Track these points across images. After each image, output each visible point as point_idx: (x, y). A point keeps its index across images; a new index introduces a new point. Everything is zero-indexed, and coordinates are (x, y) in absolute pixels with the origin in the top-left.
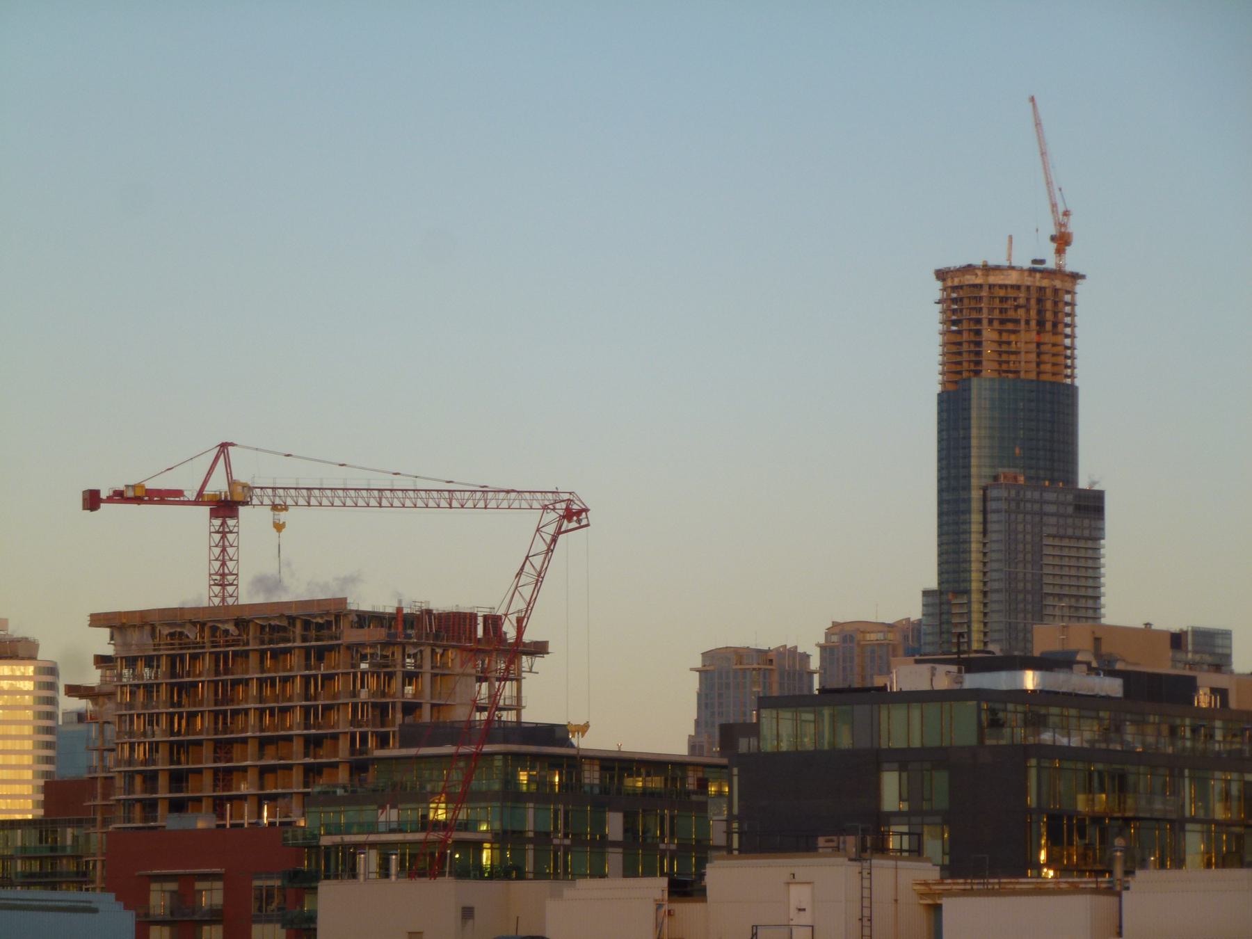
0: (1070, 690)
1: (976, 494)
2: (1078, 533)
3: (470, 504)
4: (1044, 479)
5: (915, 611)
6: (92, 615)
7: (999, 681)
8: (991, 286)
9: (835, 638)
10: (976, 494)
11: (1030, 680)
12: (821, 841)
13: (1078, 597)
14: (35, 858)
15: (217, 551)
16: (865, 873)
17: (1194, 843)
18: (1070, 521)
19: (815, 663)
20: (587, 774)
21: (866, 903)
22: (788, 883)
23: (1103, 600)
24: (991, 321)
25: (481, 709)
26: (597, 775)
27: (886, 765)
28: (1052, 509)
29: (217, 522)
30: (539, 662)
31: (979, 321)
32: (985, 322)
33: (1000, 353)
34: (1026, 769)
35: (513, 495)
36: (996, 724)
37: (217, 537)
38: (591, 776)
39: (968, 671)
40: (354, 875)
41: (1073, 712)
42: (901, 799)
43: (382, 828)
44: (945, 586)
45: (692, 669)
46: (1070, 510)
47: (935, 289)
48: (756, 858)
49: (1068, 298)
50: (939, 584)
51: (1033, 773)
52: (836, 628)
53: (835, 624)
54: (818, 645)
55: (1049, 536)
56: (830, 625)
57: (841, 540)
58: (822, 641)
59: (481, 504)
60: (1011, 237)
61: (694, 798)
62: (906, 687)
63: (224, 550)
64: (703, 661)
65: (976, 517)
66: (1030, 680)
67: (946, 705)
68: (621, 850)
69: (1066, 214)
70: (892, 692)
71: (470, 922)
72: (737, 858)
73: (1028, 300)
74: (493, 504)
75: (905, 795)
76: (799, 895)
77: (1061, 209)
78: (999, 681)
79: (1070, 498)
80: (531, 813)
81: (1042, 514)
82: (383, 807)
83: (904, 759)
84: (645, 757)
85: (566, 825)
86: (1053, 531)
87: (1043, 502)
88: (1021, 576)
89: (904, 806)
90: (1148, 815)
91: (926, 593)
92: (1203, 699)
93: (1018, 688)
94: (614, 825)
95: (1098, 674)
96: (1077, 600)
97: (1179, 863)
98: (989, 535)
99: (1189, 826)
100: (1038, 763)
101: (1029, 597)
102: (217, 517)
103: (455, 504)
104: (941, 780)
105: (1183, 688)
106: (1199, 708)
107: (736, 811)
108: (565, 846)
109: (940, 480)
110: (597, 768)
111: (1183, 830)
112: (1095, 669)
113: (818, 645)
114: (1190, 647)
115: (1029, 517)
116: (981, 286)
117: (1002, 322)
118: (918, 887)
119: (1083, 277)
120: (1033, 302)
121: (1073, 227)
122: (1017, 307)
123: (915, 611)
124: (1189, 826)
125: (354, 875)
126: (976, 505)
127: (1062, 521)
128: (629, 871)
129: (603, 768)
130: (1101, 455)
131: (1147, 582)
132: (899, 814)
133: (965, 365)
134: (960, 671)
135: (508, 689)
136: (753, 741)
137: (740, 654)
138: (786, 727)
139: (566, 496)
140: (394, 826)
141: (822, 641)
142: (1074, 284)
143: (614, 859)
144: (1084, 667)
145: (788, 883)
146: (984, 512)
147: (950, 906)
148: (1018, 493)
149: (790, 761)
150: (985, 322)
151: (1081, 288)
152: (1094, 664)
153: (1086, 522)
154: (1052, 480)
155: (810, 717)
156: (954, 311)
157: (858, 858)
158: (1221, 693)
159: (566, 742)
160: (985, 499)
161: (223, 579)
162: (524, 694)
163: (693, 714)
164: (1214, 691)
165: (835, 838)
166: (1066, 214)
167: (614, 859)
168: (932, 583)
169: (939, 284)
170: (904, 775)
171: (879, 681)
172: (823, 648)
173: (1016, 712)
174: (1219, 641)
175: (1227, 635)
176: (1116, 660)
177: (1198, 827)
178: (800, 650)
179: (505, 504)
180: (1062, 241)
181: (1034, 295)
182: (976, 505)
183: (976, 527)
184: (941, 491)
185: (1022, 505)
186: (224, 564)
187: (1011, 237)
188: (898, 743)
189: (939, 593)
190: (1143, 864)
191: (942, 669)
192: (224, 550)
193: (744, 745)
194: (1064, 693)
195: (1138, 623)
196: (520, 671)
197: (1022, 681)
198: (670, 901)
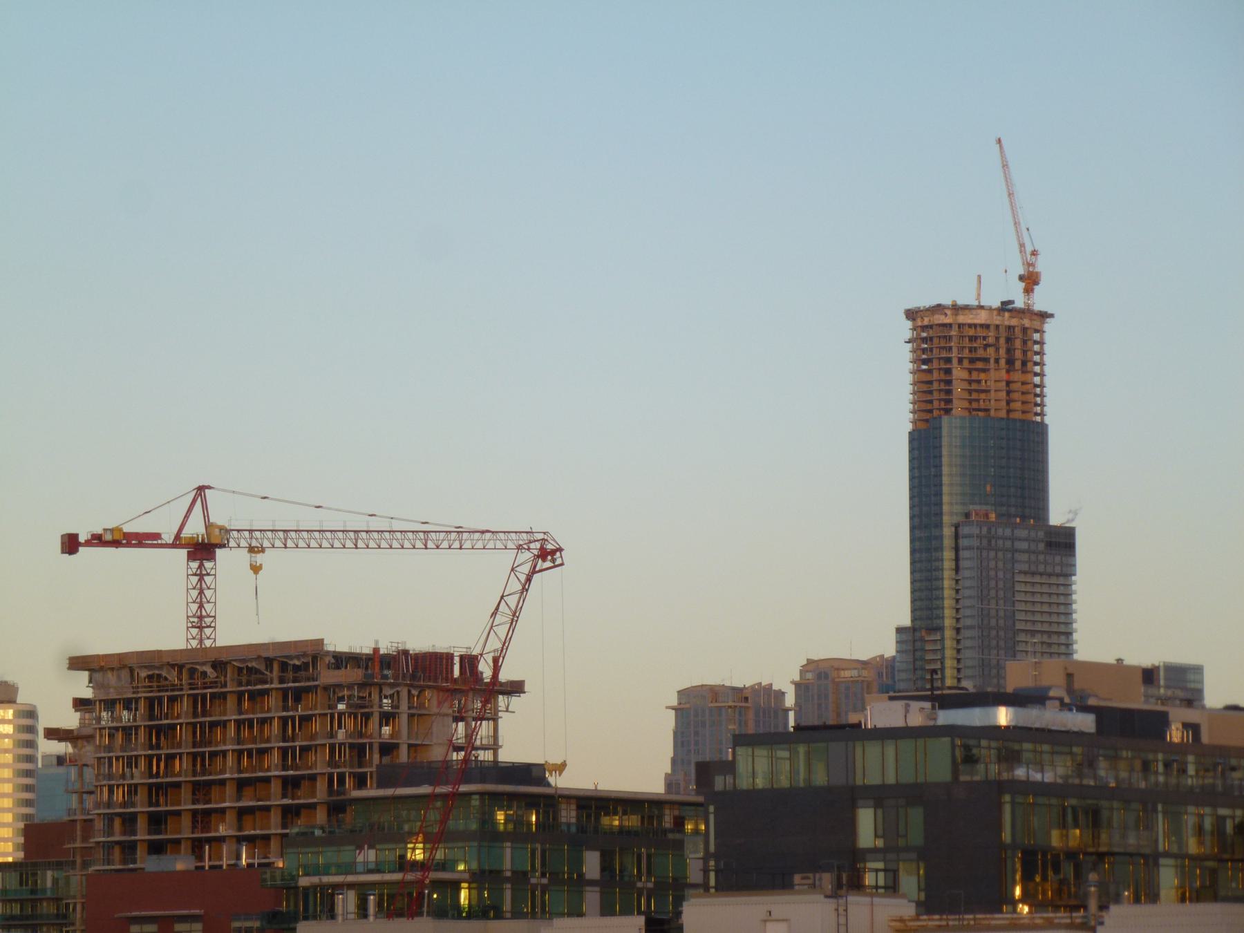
0: (1043, 726)
1: (948, 532)
3: (445, 544)
4: (1016, 516)
5: (888, 647)
6: (63, 552)
7: (972, 717)
8: (960, 325)
9: (809, 676)
10: (948, 532)
11: (1003, 716)
12: (797, 878)
13: (1049, 633)
14: (16, 901)
15: (195, 593)
16: (841, 909)
17: (1168, 878)
18: (1041, 557)
19: (790, 701)
20: (564, 813)
22: (765, 921)
23: (1075, 636)
24: (960, 361)
25: (458, 749)
26: (574, 813)
27: (860, 802)
28: (1024, 545)
29: (195, 565)
30: (515, 701)
31: (948, 360)
32: (955, 361)
33: (970, 392)
34: (1000, 806)
35: (488, 535)
36: (970, 760)
37: (195, 579)
38: (568, 815)
39: (942, 707)
40: (332, 915)
42: (876, 836)
43: (360, 868)
44: (918, 623)
45: (667, 708)
46: (1041, 546)
47: (905, 329)
48: (754, 899)
49: (1036, 336)
51: (1007, 809)
53: (810, 662)
54: (793, 682)
55: (1020, 572)
56: (805, 662)
57: (815, 578)
58: (797, 678)
59: (457, 545)
61: (670, 836)
63: (201, 592)
64: (679, 699)
65: (948, 555)
66: (1003, 716)
67: (920, 742)
68: (597, 889)
73: (997, 339)
74: (467, 545)
75: (880, 832)
77: (1029, 249)
78: (972, 717)
79: (1041, 534)
80: (508, 851)
81: (1014, 551)
82: (361, 848)
83: (879, 796)
85: (543, 864)
86: (1025, 567)
89: (880, 843)
90: (1122, 850)
91: (899, 630)
92: (1175, 734)
93: (991, 723)
95: (1071, 710)
96: (1050, 637)
99: (1162, 861)
101: (1002, 633)
102: (194, 560)
103: (430, 544)
104: (916, 816)
106: (1171, 744)
107: (712, 848)
109: (912, 518)
110: (574, 807)
111: (1157, 865)
112: (1067, 705)
113: (793, 682)
114: (1162, 682)
116: (950, 325)
118: (893, 924)
119: (1052, 316)
120: (1002, 341)
121: (1041, 266)
122: (986, 346)
123: (888, 647)
124: (1162, 861)
125: (332, 915)
126: (948, 542)
127: (1033, 557)
128: (607, 910)
129: (579, 807)
130: (1073, 490)
131: (1116, 619)
132: (875, 850)
133: (936, 403)
135: (485, 729)
136: (729, 779)
137: (714, 692)
138: (762, 765)
139: (541, 536)
140: (372, 866)
141: (797, 678)
143: (592, 897)
144: (1057, 703)
146: (957, 549)
150: (955, 361)
151: (1049, 326)
152: (1067, 700)
153: (1058, 559)
154: (1023, 517)
155: (786, 754)
156: (924, 351)
157: (834, 895)
158: (1193, 728)
159: (543, 781)
160: (957, 536)
161: (200, 622)
163: (669, 752)
164: (1186, 726)
165: (811, 875)
166: (1034, 253)
167: (592, 897)
168: (906, 621)
169: (909, 324)
170: (880, 812)
171: (853, 718)
173: (989, 748)
174: (1191, 677)
175: (1198, 670)
176: (1090, 696)
177: (1171, 861)
178: (775, 687)
179: (480, 545)
180: (1030, 280)
183: (948, 564)
184: (913, 529)
185: (993, 542)
186: (201, 606)
188: (873, 779)
189: (913, 629)
190: (1117, 899)
191: (915, 705)
192: (201, 592)
193: (720, 783)
194: (1037, 729)
196: (496, 711)
197: (995, 716)
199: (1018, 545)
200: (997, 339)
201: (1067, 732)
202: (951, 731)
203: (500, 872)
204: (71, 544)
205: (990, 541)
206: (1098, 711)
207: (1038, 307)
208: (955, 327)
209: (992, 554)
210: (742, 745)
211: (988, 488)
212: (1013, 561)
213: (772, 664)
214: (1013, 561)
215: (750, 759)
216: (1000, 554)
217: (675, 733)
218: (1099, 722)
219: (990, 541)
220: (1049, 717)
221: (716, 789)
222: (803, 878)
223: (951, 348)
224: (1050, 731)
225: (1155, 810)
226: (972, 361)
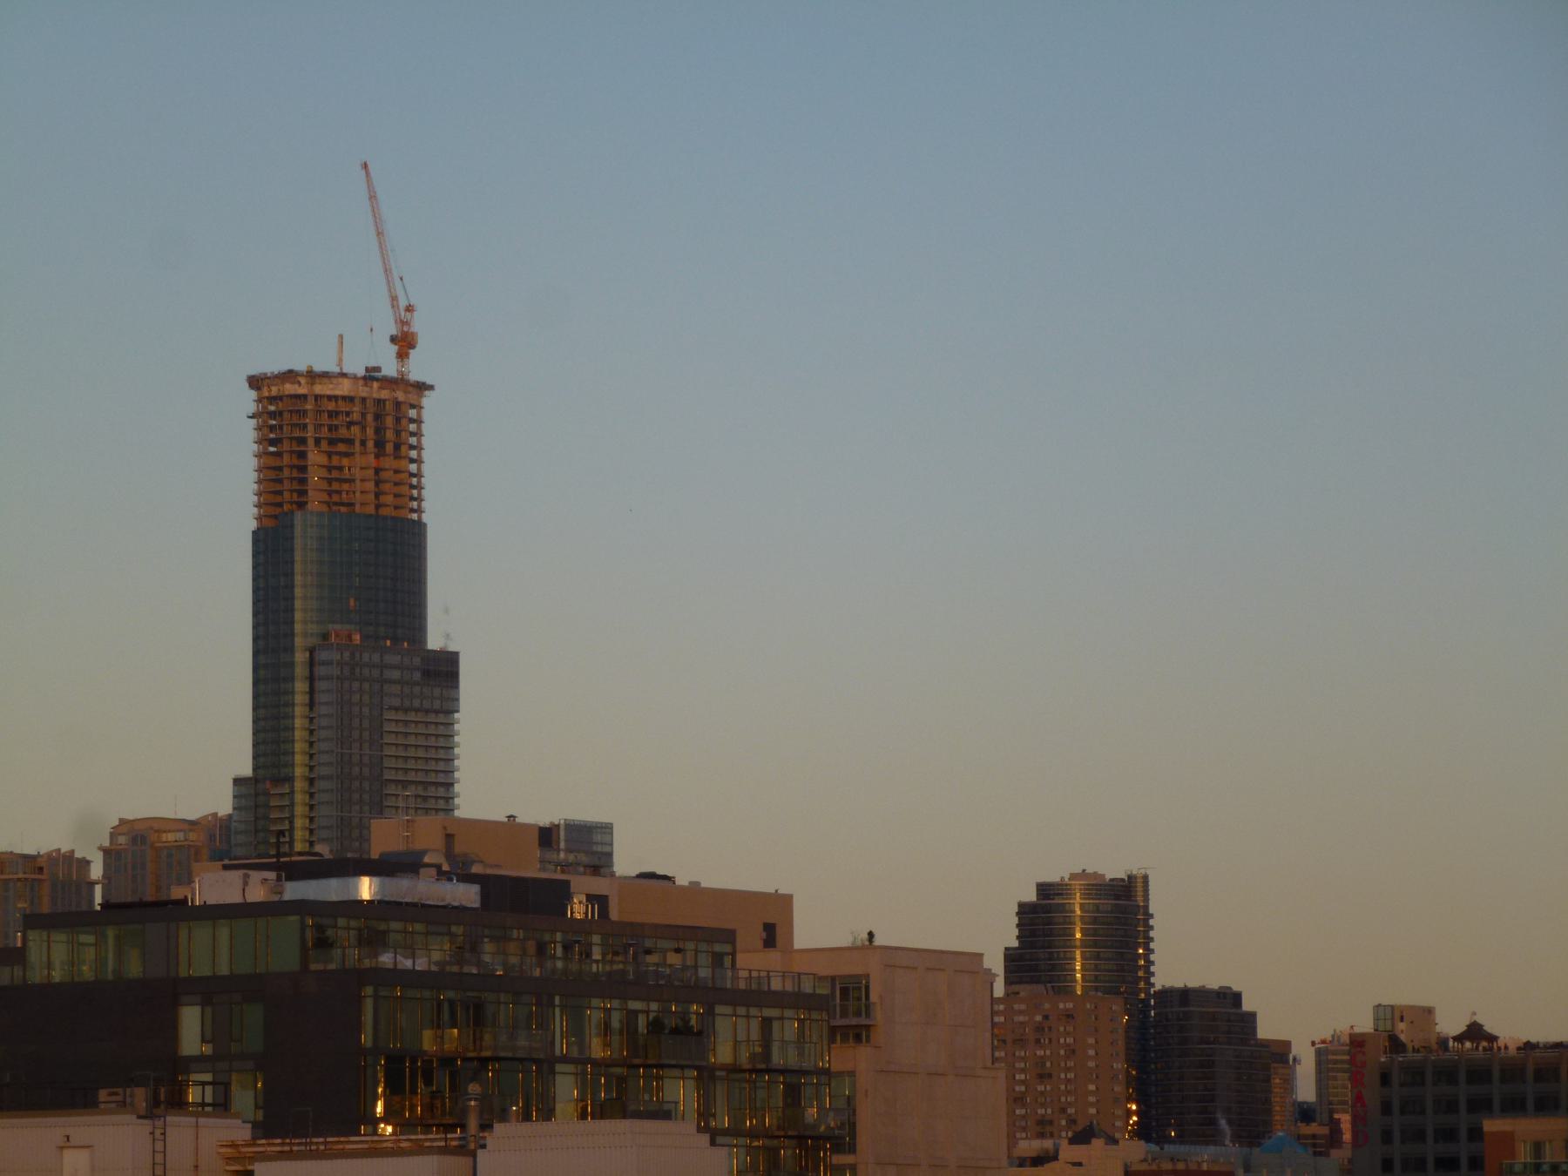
1: (300, 657)
2: (426, 704)
4: (385, 638)
5: (223, 804)
7: (327, 890)
8: (317, 397)
9: (122, 840)
10: (300, 657)
11: (366, 888)
12: (103, 1095)
13: (425, 784)
17: (566, 1089)
18: (417, 689)
19: (96, 871)
23: (457, 788)
24: (317, 441)
28: (396, 674)
31: (303, 441)
32: (311, 442)
36: (323, 943)
39: (289, 878)
41: (419, 927)
42: (203, 1041)
46: (417, 676)
49: (413, 413)
50: (255, 769)
51: (369, 1005)
54: (101, 848)
58: (107, 843)
60: (341, 337)
65: (300, 686)
66: (366, 888)
69: (410, 309)
73: (363, 415)
77: (403, 303)
78: (327, 890)
79: (417, 661)
83: (208, 991)
88: (356, 759)
90: (510, 1055)
91: (238, 781)
95: (450, 880)
97: (548, 1114)
99: (559, 1067)
100: (376, 991)
101: (366, 785)
111: (553, 1072)
113: (101, 848)
114: (562, 845)
116: (305, 397)
117: (332, 442)
118: (223, 1150)
119: (431, 388)
120: (370, 417)
121: (418, 325)
123: (223, 804)
124: (559, 1067)
126: (300, 671)
131: (507, 767)
132: (200, 1059)
134: (279, 879)
136: (18, 971)
142: (421, 396)
144: (433, 871)
146: (311, 679)
150: (311, 442)
151: (428, 401)
152: (446, 868)
153: (437, 691)
154: (395, 640)
156: (272, 428)
157: (149, 1115)
160: (311, 663)
165: (120, 1090)
166: (409, 309)
168: (246, 770)
170: (209, 1010)
172: (107, 852)
174: (598, 838)
175: (607, 828)
176: (473, 862)
177: (570, 1068)
180: (404, 342)
181: (371, 408)
182: (300, 671)
183: (300, 698)
184: (256, 653)
187: (341, 337)
188: (202, 969)
190: (503, 1116)
191: (256, 876)
195: (499, 816)
197: (356, 889)
199: (389, 674)
200: (363, 415)
207: (415, 375)
208: (311, 400)
209: (356, 685)
211: (352, 602)
216: (366, 686)
218: (485, 896)
220: (425, 889)
222: (110, 1094)
223: (305, 426)
224: (400, 904)
226: (332, 442)
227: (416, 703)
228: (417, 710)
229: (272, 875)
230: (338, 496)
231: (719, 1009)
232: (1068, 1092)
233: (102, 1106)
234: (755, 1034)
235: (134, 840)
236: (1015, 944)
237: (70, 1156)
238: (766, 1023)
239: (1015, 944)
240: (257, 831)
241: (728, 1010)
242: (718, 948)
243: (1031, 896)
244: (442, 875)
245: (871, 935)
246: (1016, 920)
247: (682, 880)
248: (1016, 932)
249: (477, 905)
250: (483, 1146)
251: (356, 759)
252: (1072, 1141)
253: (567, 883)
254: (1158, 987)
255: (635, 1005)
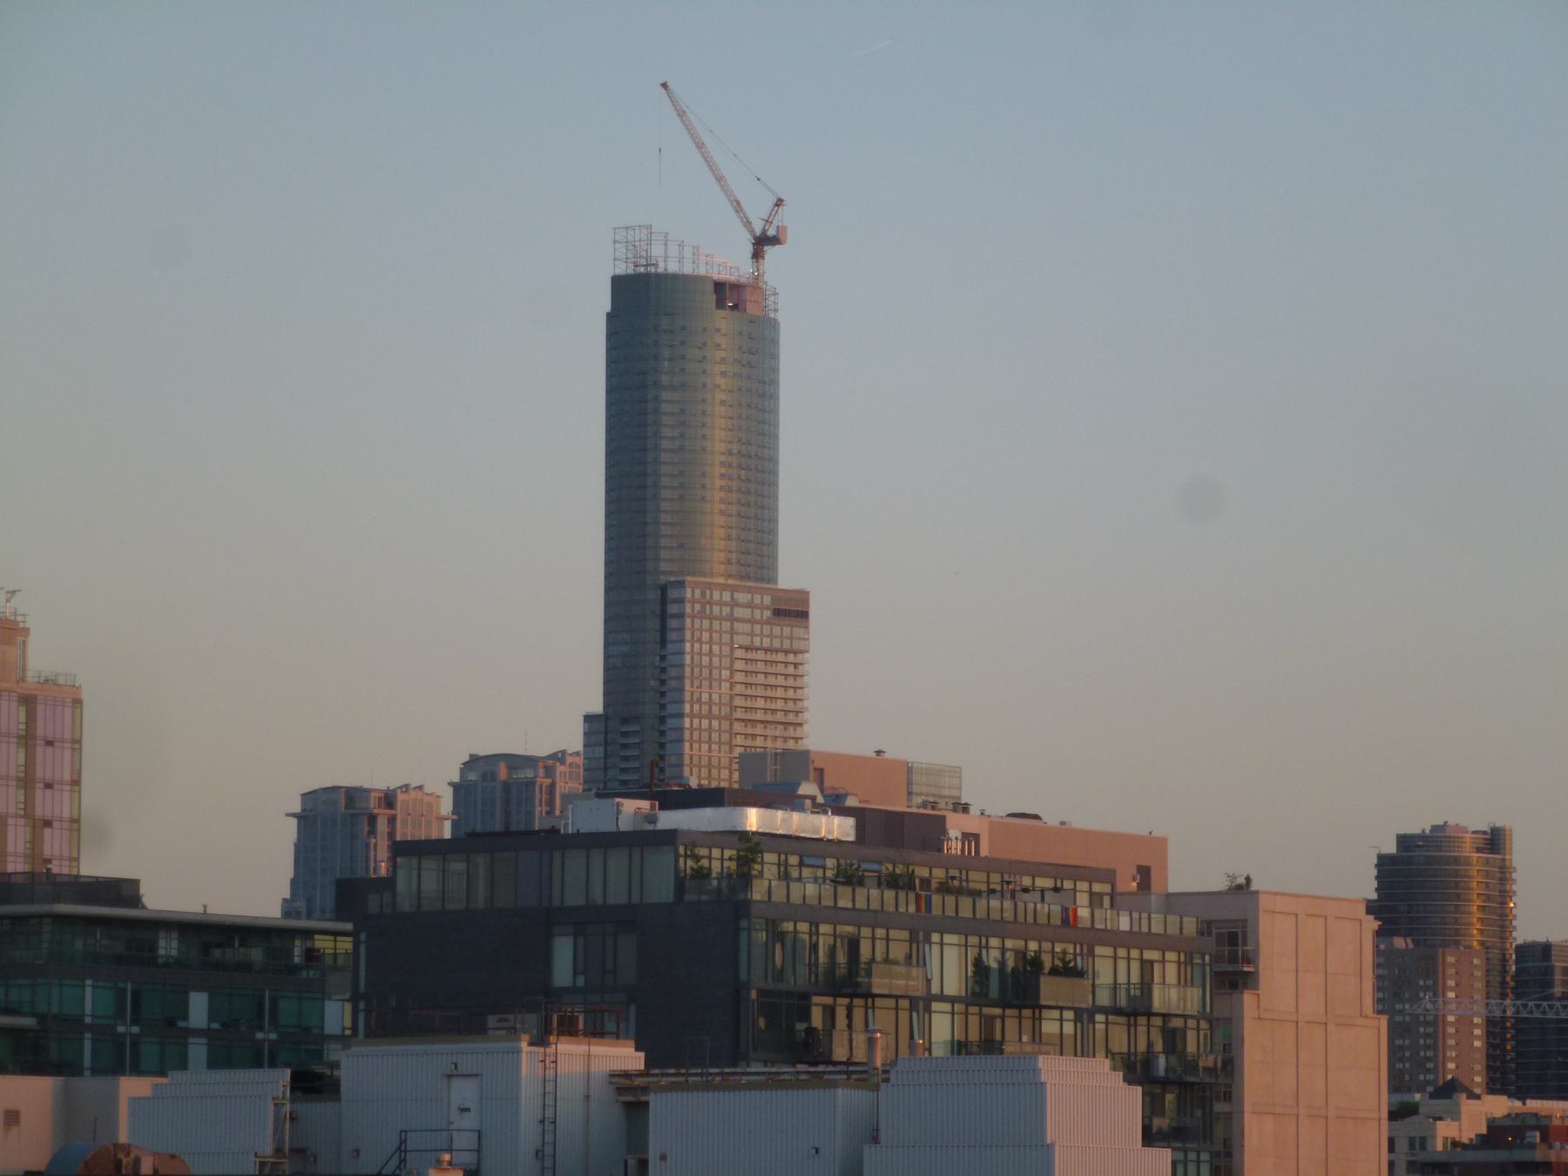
2: (777, 644)
5: (572, 739)
9: (472, 777)
12: (492, 1020)
18: (767, 629)
19: (446, 806)
21: (550, 1101)
22: (450, 1076)
38: (168, 947)
42: (575, 973)
46: (767, 614)
50: (605, 707)
52: (306, 796)
53: (474, 761)
62: (586, 828)
64: (304, 803)
67: (597, 857)
68: (204, 1041)
70: (567, 835)
71: (14, 1131)
72: (1257, 967)
76: (463, 1092)
79: (767, 600)
81: (732, 619)
83: (582, 921)
84: (239, 921)
86: (746, 641)
87: (734, 604)
90: (886, 992)
91: (588, 718)
94: (198, 1008)
95: (825, 813)
96: (754, 727)
97: (183, 1064)
98: (669, 646)
99: (935, 1006)
105: (937, 826)
106: (949, 856)
107: (362, 988)
108: (132, 1035)
111: (928, 1010)
112: (821, 805)
115: (716, 624)
124: (935, 1006)
127: (757, 628)
132: (573, 990)
143: (198, 1051)
144: (808, 802)
145: (450, 1076)
147: (659, 1105)
148: (703, 594)
149: (442, 921)
152: (820, 800)
153: (787, 630)
162: (699, 156)
163: (289, 873)
164: (966, 836)
167: (198, 1051)
168: (597, 707)
170: (581, 941)
172: (457, 788)
176: (846, 795)
177: (947, 1007)
184: (609, 589)
188: (574, 899)
193: (373, 903)
198: (293, 1100)
199: (740, 612)
201: (821, 840)
202: (670, 837)
203: (78, 1020)
204: (664, 85)
205: (703, 607)
206: (859, 814)
209: (706, 623)
210: (402, 855)
212: (732, 633)
213: (416, 760)
214: (732, 633)
215: (415, 873)
217: (296, 845)
218: (860, 829)
219: (703, 607)
221: (851, 837)
222: (501, 1020)
225: (928, 941)
227: (766, 642)
228: (766, 650)
229: (645, 805)
230: (671, 351)
231: (1099, 950)
232: (1427, 1047)
233: (491, 1032)
234: (1135, 978)
235: (484, 777)
236: (1374, 896)
237: (457, 1084)
238: (1146, 966)
239: (1374, 896)
240: (606, 769)
241: (1108, 951)
242: (1097, 888)
243: (1391, 848)
244: (819, 809)
245: (1248, 879)
246: (1375, 872)
247: (1051, 819)
248: (1375, 884)
249: (852, 838)
250: (888, 1080)
251: (705, 697)
252: (1433, 1096)
253: (944, 818)
254: (1520, 941)
255: (1009, 944)
